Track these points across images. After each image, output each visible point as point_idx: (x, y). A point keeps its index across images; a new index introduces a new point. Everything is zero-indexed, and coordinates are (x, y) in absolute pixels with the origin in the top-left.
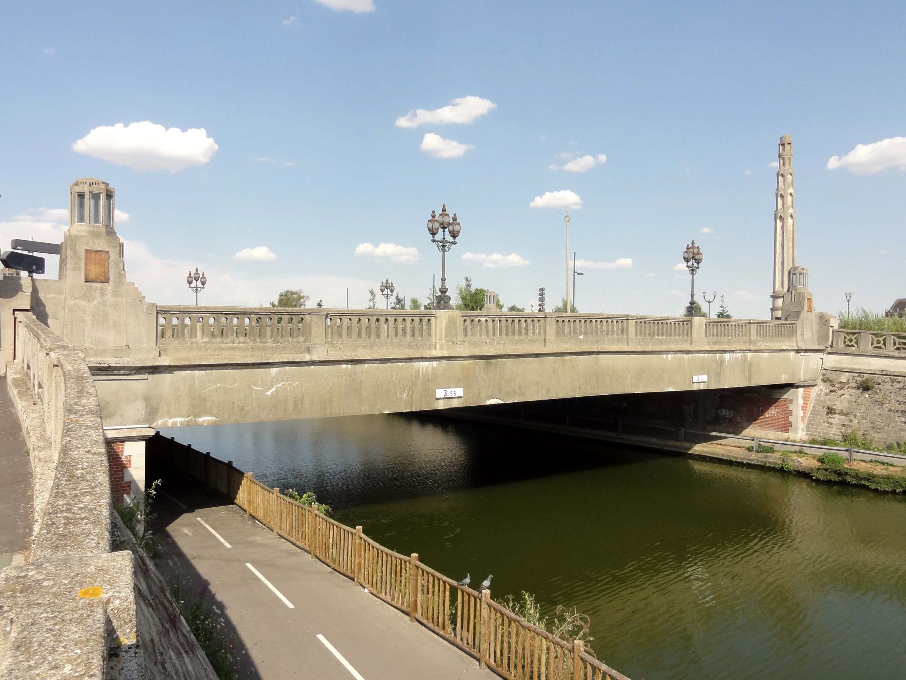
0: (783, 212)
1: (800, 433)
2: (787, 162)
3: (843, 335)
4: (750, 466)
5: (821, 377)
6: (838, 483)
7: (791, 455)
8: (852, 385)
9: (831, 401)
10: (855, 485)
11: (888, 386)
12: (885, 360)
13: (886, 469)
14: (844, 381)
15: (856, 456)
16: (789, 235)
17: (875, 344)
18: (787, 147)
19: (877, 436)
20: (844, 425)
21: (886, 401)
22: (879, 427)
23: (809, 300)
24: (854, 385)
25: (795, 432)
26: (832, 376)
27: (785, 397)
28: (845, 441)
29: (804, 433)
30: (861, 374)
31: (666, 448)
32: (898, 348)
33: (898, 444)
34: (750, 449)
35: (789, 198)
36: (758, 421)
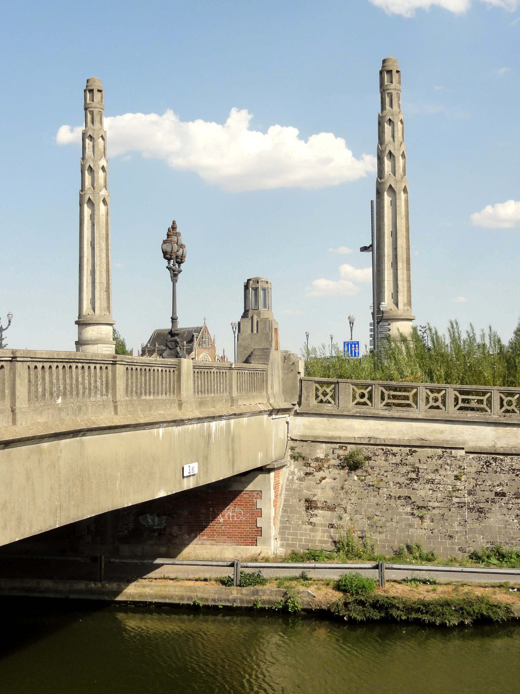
0: (93, 194)
1: (272, 546)
3: (315, 385)
4: (230, 611)
5: (289, 452)
6: (370, 622)
7: (294, 583)
8: (333, 462)
9: (308, 488)
10: (407, 623)
11: (380, 461)
12: (372, 423)
13: (434, 590)
14: (322, 456)
15: (389, 574)
17: (432, 403)
18: (97, 96)
19: (377, 537)
20: (332, 526)
21: (382, 484)
22: (379, 524)
23: (276, 329)
24: (337, 462)
25: (270, 544)
26: (303, 449)
27: (250, 487)
28: (339, 550)
29: (279, 543)
30: (343, 444)
31: (72, 596)
32: (387, 405)
33: (408, 547)
34: (225, 582)
35: (101, 174)
36: (207, 530)
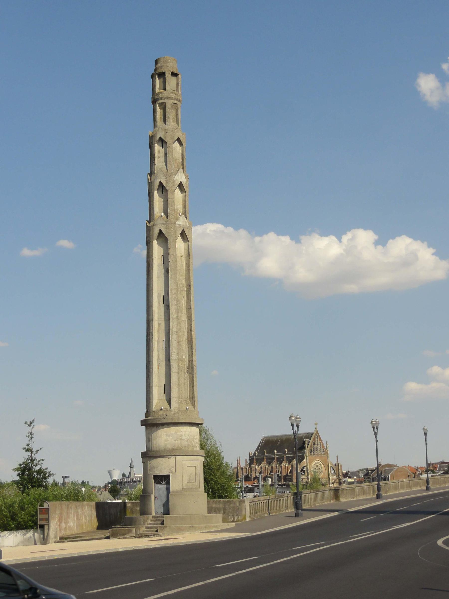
0: (166, 224)
2: (171, 114)
16: (178, 280)
18: (171, 82)
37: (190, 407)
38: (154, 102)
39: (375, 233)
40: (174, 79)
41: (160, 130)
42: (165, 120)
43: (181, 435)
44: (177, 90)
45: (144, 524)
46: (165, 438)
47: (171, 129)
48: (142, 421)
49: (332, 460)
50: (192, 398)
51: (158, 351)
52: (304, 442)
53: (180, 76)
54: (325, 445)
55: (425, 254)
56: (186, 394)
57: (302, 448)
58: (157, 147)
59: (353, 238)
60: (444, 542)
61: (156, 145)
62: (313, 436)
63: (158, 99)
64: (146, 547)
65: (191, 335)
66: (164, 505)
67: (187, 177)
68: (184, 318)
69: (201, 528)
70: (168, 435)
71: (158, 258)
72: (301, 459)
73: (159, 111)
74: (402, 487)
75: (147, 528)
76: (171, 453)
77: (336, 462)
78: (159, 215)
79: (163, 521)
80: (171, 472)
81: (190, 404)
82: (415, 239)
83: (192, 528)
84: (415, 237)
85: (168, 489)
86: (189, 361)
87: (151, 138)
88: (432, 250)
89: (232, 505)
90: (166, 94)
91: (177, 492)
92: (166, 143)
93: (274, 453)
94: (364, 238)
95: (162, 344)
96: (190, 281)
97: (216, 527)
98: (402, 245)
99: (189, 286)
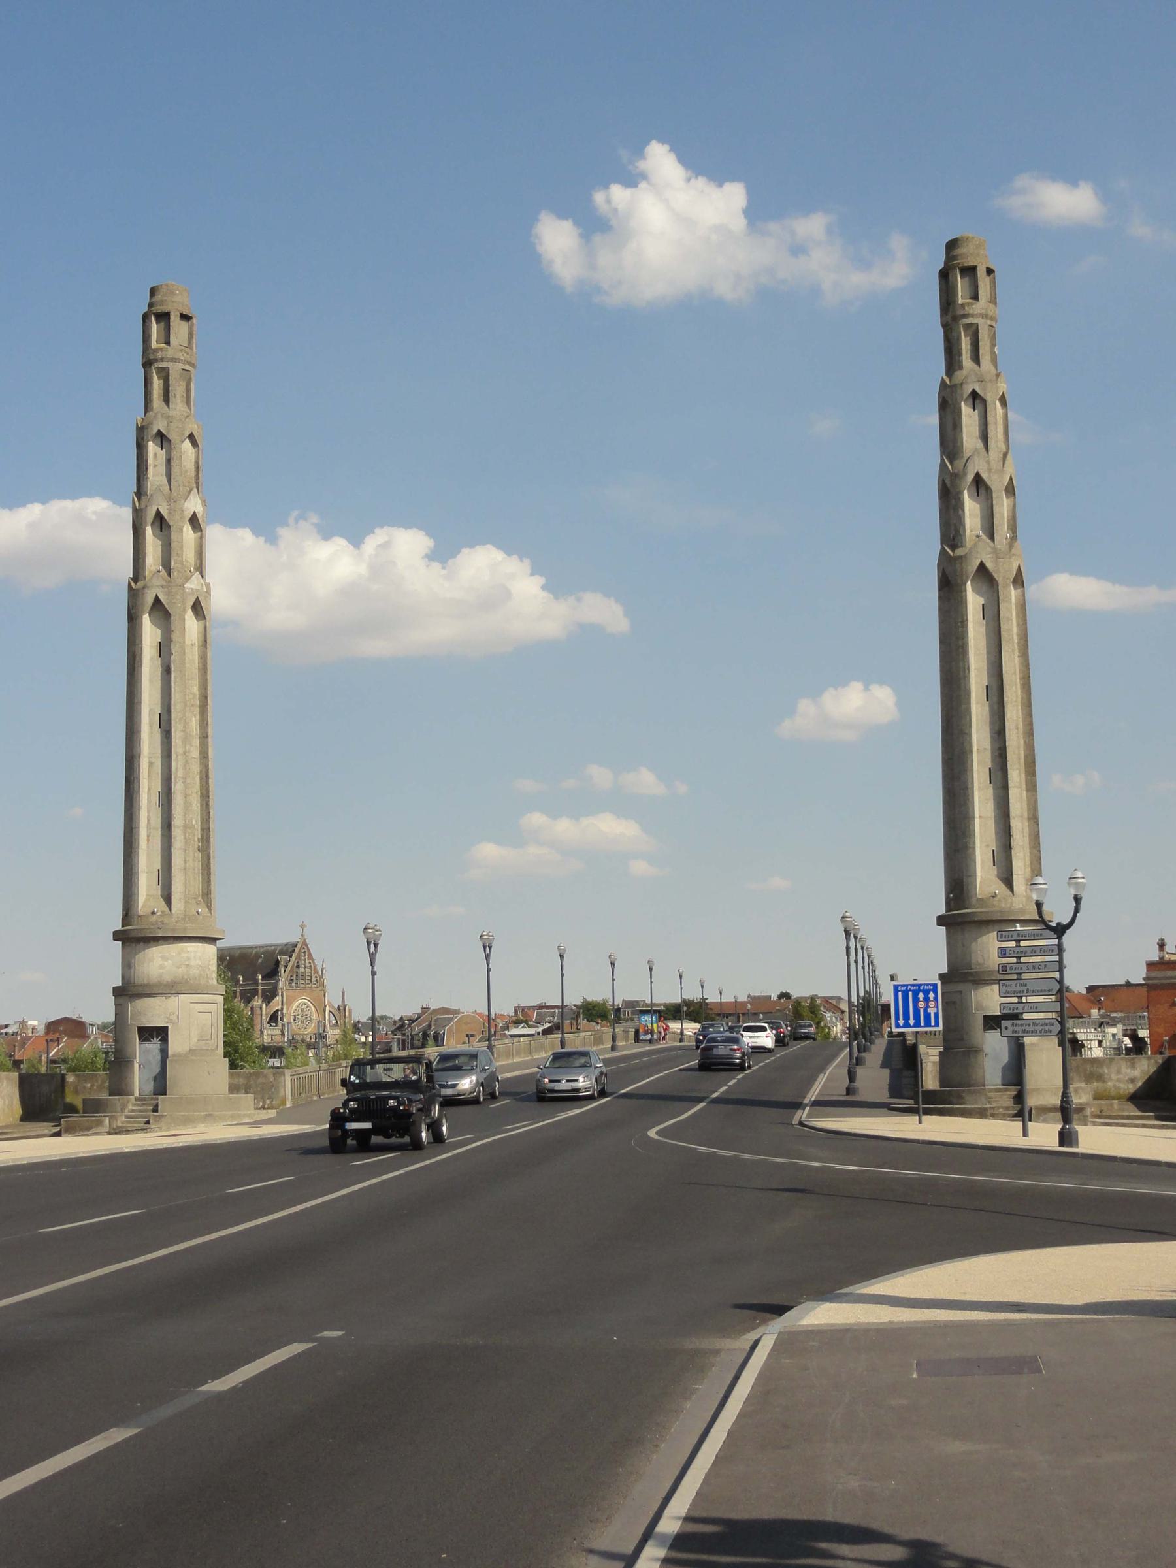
0: (168, 586)
2: (177, 389)
18: (179, 330)
37: (203, 909)
38: (147, 364)
39: (429, 534)
40: (184, 325)
41: (159, 416)
42: (166, 399)
43: (188, 959)
44: (190, 346)
45: (122, 1111)
46: (158, 962)
47: (175, 416)
48: (115, 933)
49: (333, 999)
50: (207, 894)
51: (148, 812)
52: (277, 963)
53: (194, 321)
54: (319, 968)
55: (527, 588)
56: (197, 886)
57: (272, 972)
58: (152, 447)
59: (386, 546)
60: (657, 1133)
61: (150, 443)
62: (297, 950)
63: (156, 360)
64: (165, 1146)
65: (207, 783)
66: (155, 1079)
67: (204, 503)
68: (195, 753)
69: (223, 1118)
70: (164, 958)
71: (151, 647)
72: (269, 997)
73: (157, 383)
74: (518, 1053)
75: (127, 1117)
76: (172, 989)
77: (340, 1003)
78: (154, 569)
79: (157, 1105)
80: (170, 1021)
81: (204, 904)
82: (509, 552)
83: (209, 1118)
84: (508, 549)
85: (164, 1052)
86: (202, 830)
87: (141, 431)
88: (539, 580)
89: (261, 1080)
90: (170, 352)
91: (179, 1055)
92: (169, 441)
93: (256, 983)
94: (408, 545)
95: (155, 799)
96: (206, 689)
97: (249, 1116)
98: (483, 564)
99: (204, 698)
